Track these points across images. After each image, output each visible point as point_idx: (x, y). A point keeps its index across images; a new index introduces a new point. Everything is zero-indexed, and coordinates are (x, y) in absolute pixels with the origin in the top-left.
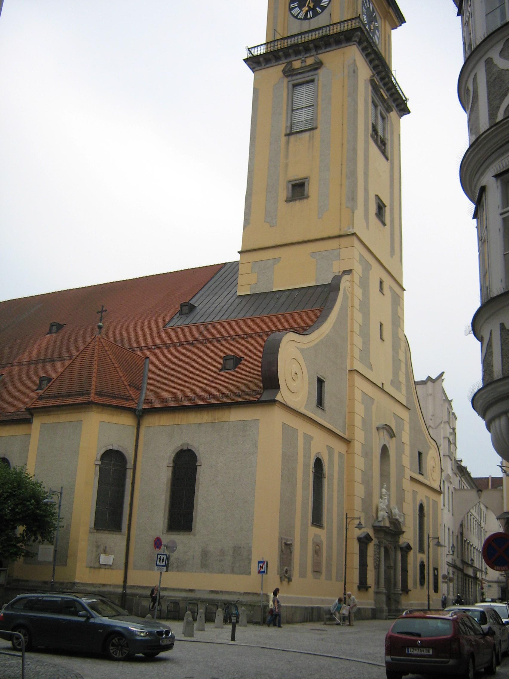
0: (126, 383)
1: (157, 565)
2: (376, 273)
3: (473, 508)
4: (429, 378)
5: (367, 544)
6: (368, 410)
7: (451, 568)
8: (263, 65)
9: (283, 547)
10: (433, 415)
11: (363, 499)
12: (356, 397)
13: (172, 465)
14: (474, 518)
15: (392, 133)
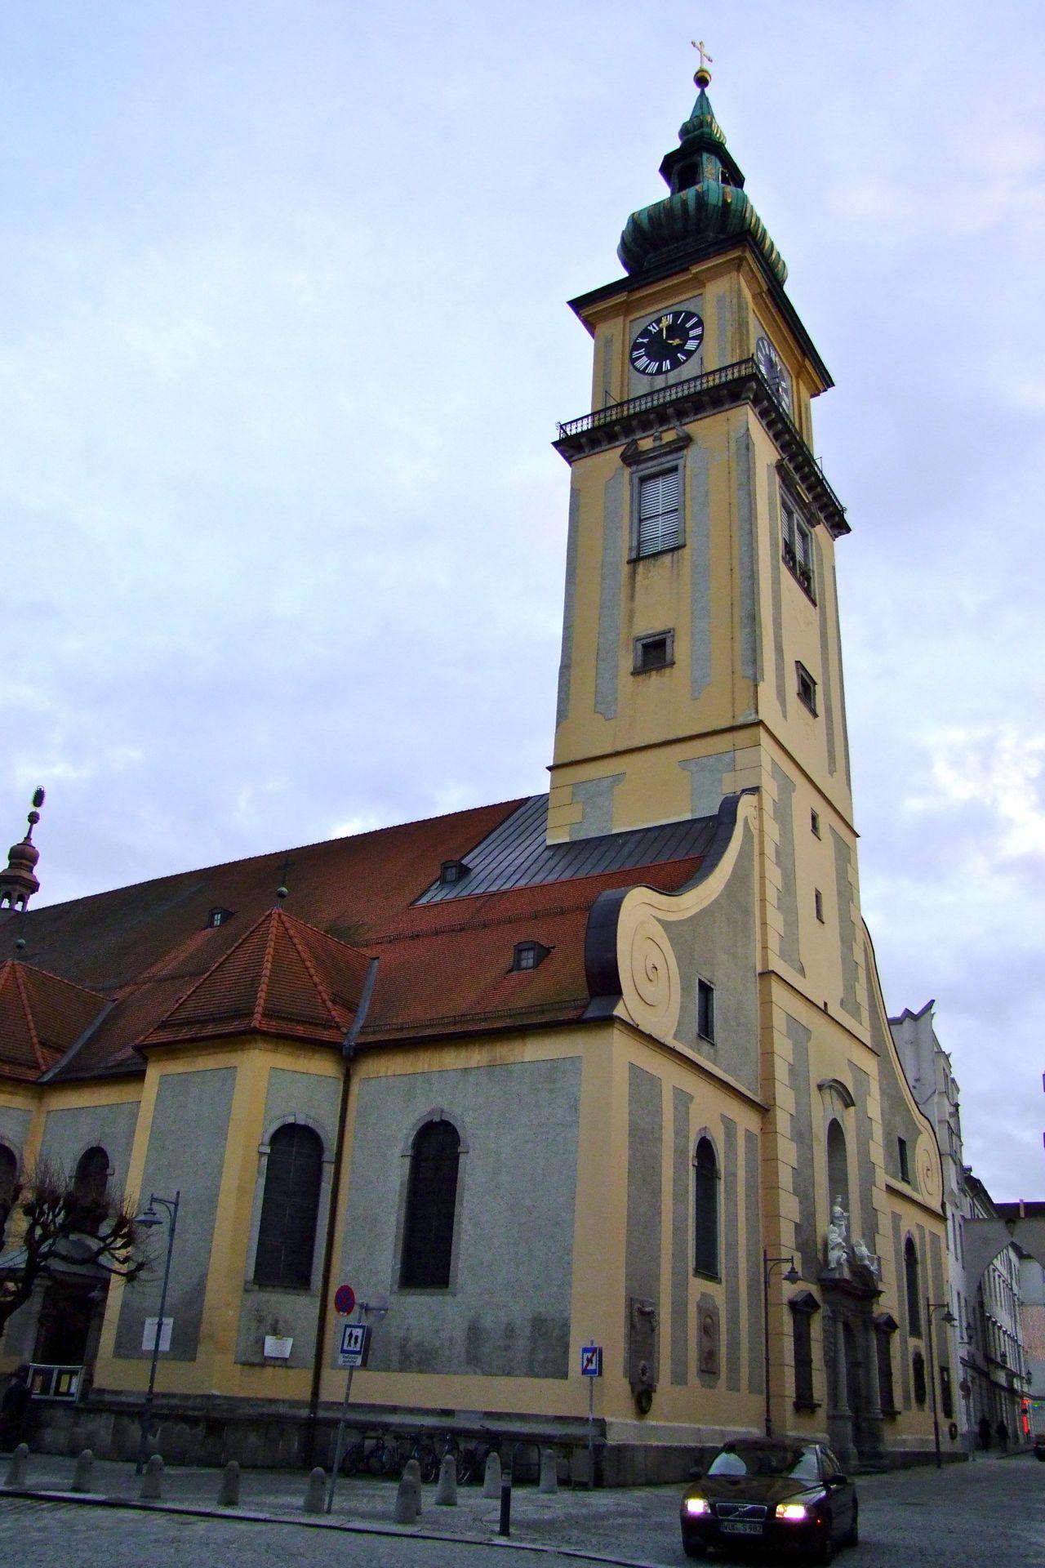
0: (325, 997)
1: (343, 1351)
2: (804, 801)
3: (996, 1257)
4: (907, 1013)
5: (808, 1316)
6: (800, 1050)
7: (969, 1370)
8: (587, 451)
9: (636, 1319)
10: (917, 1080)
11: (796, 1224)
12: (777, 1076)
13: (410, 1152)
14: (999, 1277)
15: (821, 561)
